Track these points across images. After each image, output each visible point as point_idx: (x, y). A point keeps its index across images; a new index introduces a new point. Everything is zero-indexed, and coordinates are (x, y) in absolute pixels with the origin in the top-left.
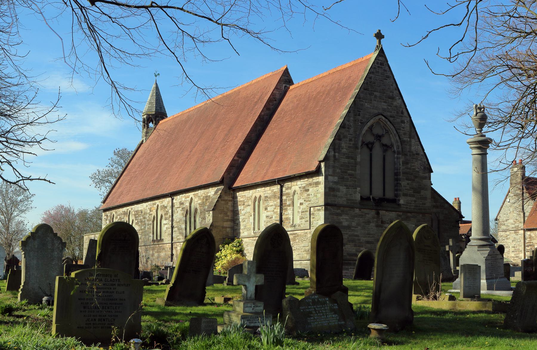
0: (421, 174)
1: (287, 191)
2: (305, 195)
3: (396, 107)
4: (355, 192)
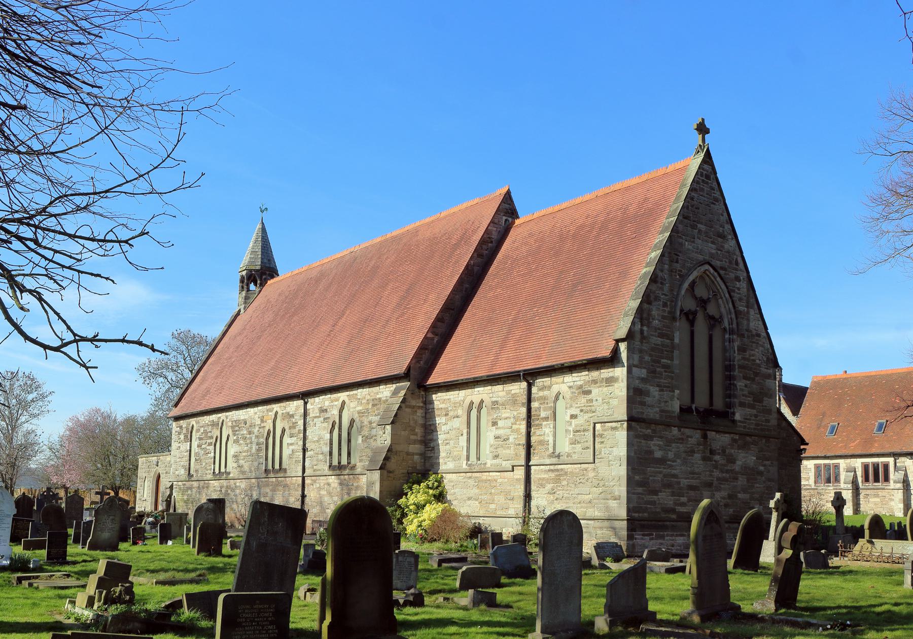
0: (763, 370)
1: (541, 394)
2: (583, 400)
3: (728, 252)
4: (672, 398)
